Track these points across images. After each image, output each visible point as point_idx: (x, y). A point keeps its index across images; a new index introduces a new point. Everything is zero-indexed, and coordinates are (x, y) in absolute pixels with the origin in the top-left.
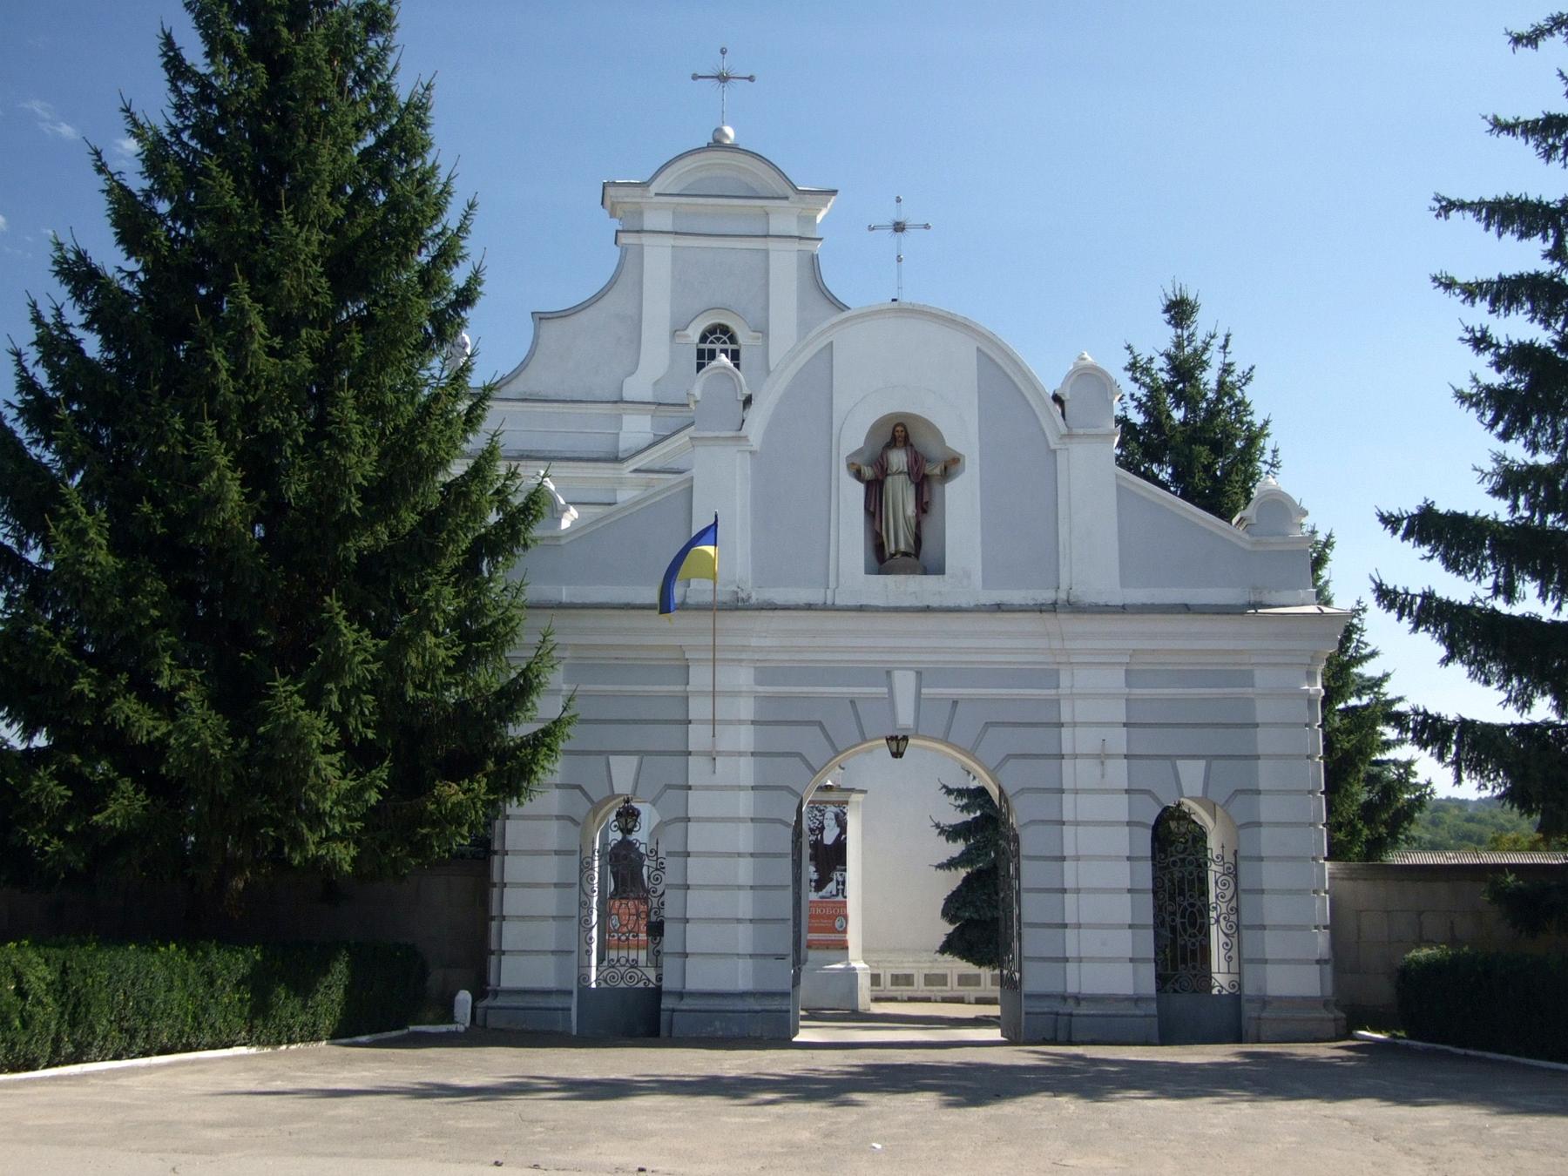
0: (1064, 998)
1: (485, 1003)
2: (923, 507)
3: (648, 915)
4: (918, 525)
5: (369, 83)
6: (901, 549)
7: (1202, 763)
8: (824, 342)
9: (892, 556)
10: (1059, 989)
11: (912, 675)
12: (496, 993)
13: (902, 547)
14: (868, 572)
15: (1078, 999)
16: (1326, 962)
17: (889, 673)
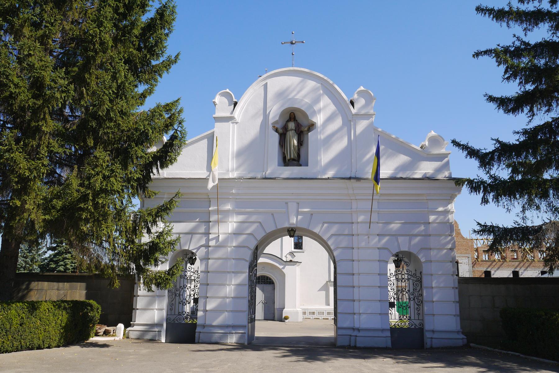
0: (353, 329)
1: (129, 329)
2: (301, 143)
3: (194, 295)
4: (299, 150)
5: (93, 213)
6: (293, 158)
7: (408, 237)
8: (264, 83)
9: (289, 160)
10: (351, 326)
11: (295, 204)
12: (134, 325)
13: (292, 156)
14: (279, 165)
15: (359, 330)
16: (456, 288)
17: (287, 203)
